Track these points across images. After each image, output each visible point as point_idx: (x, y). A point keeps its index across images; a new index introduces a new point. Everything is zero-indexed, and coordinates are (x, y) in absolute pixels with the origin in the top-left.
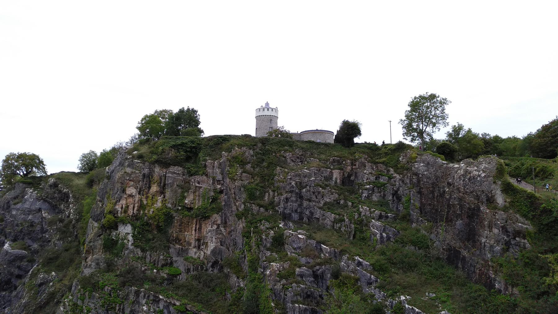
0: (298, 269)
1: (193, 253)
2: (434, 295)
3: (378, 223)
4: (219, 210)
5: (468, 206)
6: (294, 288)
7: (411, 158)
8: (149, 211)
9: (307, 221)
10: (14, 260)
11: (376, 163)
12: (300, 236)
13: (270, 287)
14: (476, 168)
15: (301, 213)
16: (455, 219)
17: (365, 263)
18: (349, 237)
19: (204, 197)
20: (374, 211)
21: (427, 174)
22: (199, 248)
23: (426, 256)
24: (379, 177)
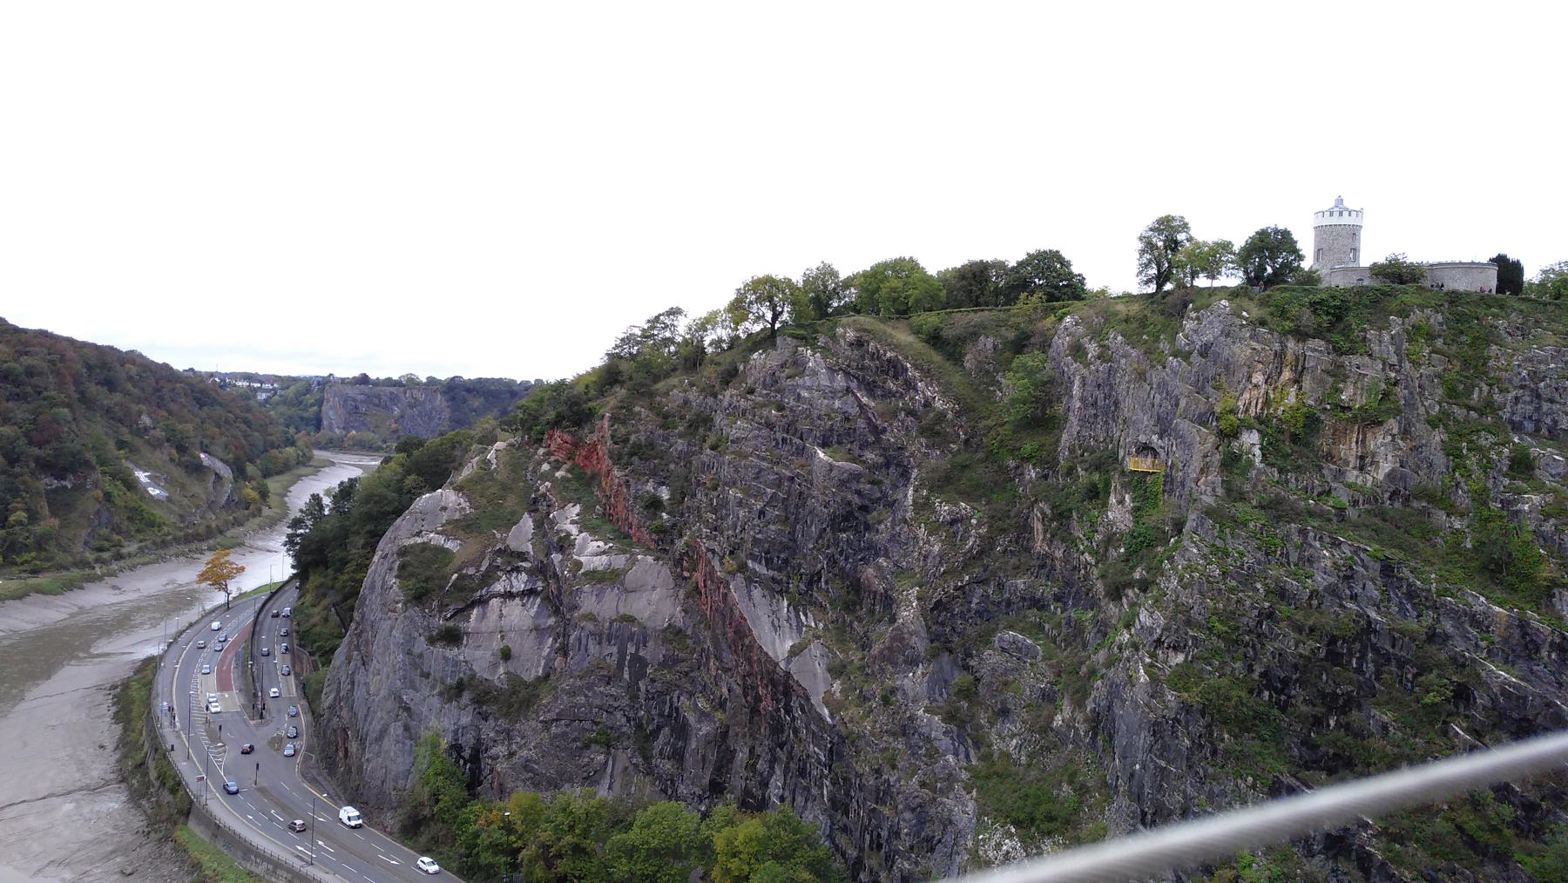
4: (1397, 412)
12: (1556, 457)
13: (1531, 528)
15: (1538, 421)
19: (1369, 390)
22: (1361, 469)
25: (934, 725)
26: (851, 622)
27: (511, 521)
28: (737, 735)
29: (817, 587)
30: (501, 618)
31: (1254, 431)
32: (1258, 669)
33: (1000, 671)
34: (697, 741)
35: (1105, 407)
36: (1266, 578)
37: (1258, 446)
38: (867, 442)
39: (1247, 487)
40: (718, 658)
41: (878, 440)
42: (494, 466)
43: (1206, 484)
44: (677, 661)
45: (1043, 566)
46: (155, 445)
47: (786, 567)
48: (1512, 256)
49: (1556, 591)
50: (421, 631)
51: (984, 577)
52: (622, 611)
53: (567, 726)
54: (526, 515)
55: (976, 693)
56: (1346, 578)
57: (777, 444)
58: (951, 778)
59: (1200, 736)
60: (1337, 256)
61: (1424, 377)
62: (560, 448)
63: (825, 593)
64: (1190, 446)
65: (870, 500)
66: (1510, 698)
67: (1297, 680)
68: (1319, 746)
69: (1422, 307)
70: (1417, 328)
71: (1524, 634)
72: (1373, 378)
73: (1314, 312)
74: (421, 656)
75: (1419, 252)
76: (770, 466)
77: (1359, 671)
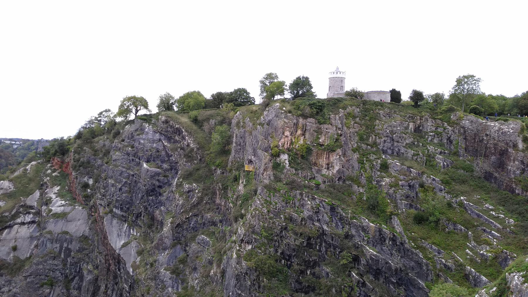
1: (324, 171)
2: (479, 197)
3: (441, 157)
4: (341, 146)
5: (500, 148)
7: (460, 118)
8: (295, 146)
9: (396, 154)
10: (154, 176)
11: (435, 119)
12: (397, 163)
13: (385, 192)
14: (506, 127)
15: (393, 150)
16: (491, 155)
17: (437, 179)
19: (331, 138)
20: (437, 149)
21: (471, 128)
22: (328, 169)
23: (471, 176)
24: (437, 128)
25: (165, 274)
26: (150, 232)
27: (31, 193)
28: (101, 279)
29: (140, 219)
30: (17, 233)
32: (280, 251)
33: (196, 252)
34: (86, 283)
35: (242, 147)
37: (287, 160)
38: (165, 160)
39: (283, 176)
40: (98, 248)
41: (169, 159)
42: (29, 171)
43: (266, 175)
44: (84, 249)
45: (218, 209)
47: (128, 211)
49: (393, 216)
52: (64, 229)
54: (37, 190)
55: (186, 261)
56: (316, 212)
57: (130, 161)
59: (254, 280)
62: (56, 164)
63: (142, 221)
64: (261, 160)
65: (163, 183)
66: (373, 260)
67: (295, 255)
68: (302, 283)
69: (351, 106)
70: (349, 114)
71: (380, 234)
72: (332, 133)
73: (311, 108)
75: (363, 88)
76: (126, 170)
77: (320, 251)
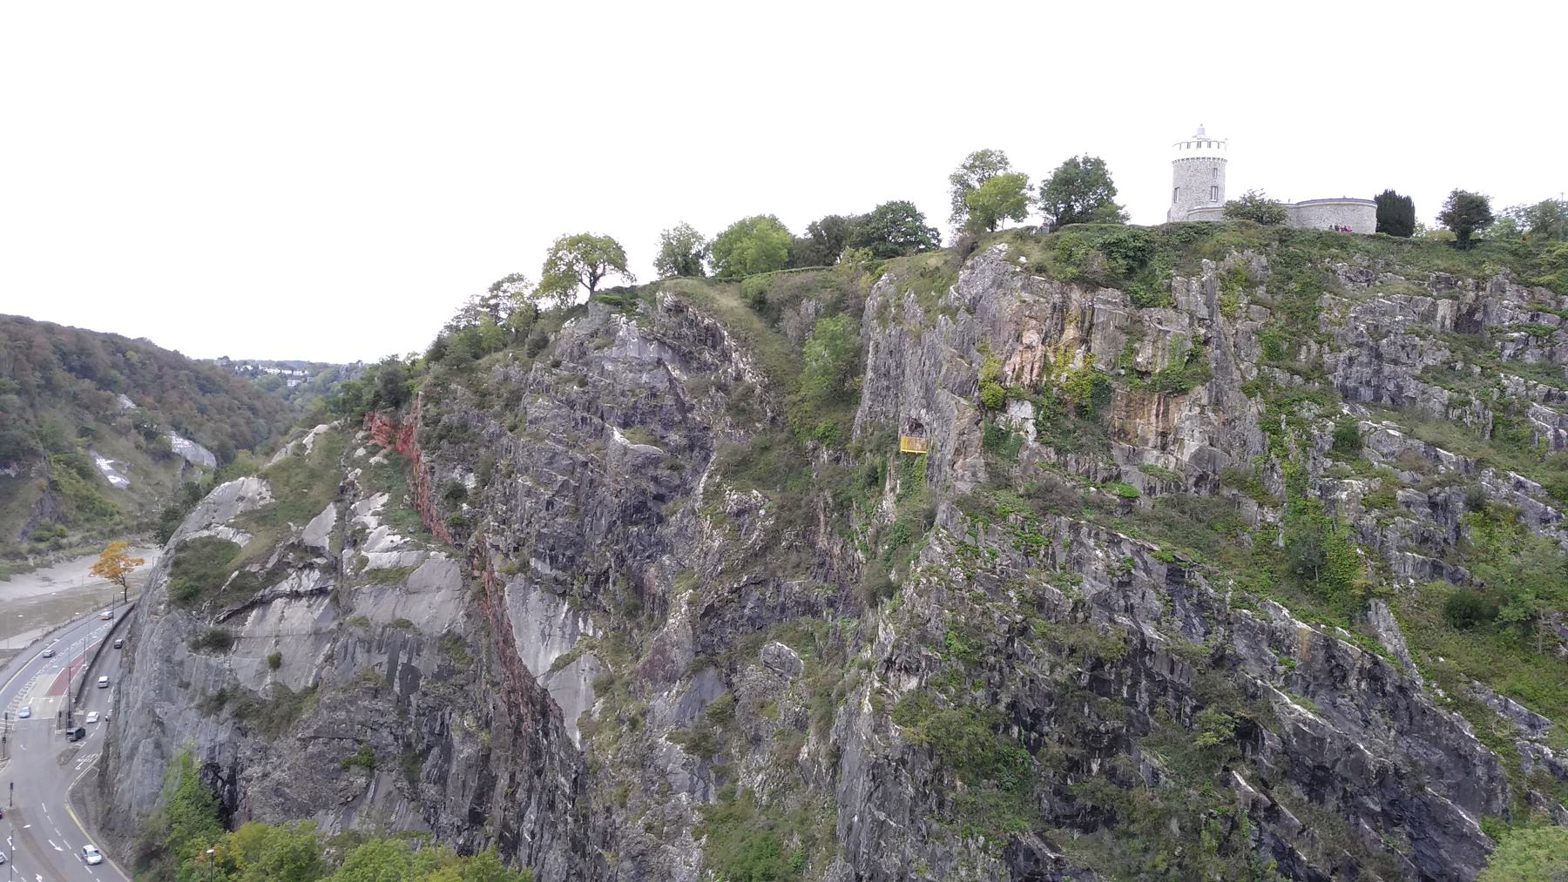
0: (1400, 492)
3: (1547, 410)
4: (1206, 378)
6: (1400, 525)
8: (1058, 376)
9: (1390, 402)
10: (643, 466)
11: (1529, 285)
12: (1391, 432)
13: (1349, 522)
15: (1378, 387)
17: (1530, 483)
18: (1483, 435)
19: (1173, 350)
20: (1535, 386)
22: (1164, 448)
24: (1538, 316)
25: (672, 753)
27: (314, 511)
28: (499, 758)
31: (1027, 403)
32: (1005, 699)
33: (759, 689)
36: (1021, 585)
37: (1032, 421)
39: (1016, 471)
41: (685, 419)
42: (308, 451)
44: (453, 672)
45: (822, 565)
46: (122, 432)
48: (1401, 192)
49: (1372, 602)
50: (184, 636)
51: (763, 577)
52: (399, 615)
53: (325, 744)
54: (331, 505)
56: (1121, 584)
57: (577, 424)
58: (680, 821)
59: (925, 783)
60: (1195, 196)
61: (1240, 334)
62: (379, 430)
64: (947, 422)
65: (667, 487)
66: (1303, 739)
67: (1051, 714)
68: (1074, 798)
69: (1241, 248)
71: (1330, 657)
73: (1110, 254)
74: (181, 663)
77: (1131, 702)
